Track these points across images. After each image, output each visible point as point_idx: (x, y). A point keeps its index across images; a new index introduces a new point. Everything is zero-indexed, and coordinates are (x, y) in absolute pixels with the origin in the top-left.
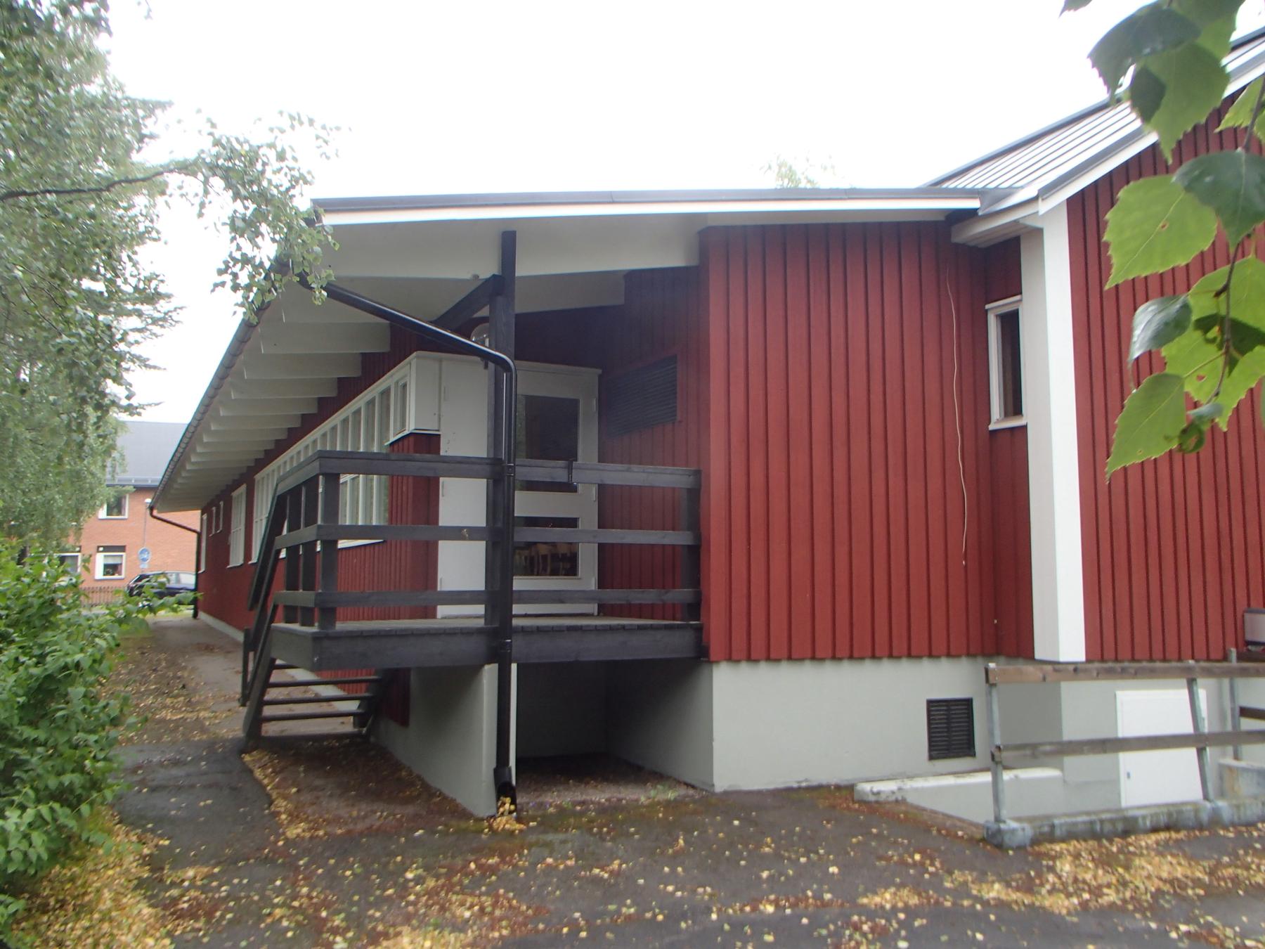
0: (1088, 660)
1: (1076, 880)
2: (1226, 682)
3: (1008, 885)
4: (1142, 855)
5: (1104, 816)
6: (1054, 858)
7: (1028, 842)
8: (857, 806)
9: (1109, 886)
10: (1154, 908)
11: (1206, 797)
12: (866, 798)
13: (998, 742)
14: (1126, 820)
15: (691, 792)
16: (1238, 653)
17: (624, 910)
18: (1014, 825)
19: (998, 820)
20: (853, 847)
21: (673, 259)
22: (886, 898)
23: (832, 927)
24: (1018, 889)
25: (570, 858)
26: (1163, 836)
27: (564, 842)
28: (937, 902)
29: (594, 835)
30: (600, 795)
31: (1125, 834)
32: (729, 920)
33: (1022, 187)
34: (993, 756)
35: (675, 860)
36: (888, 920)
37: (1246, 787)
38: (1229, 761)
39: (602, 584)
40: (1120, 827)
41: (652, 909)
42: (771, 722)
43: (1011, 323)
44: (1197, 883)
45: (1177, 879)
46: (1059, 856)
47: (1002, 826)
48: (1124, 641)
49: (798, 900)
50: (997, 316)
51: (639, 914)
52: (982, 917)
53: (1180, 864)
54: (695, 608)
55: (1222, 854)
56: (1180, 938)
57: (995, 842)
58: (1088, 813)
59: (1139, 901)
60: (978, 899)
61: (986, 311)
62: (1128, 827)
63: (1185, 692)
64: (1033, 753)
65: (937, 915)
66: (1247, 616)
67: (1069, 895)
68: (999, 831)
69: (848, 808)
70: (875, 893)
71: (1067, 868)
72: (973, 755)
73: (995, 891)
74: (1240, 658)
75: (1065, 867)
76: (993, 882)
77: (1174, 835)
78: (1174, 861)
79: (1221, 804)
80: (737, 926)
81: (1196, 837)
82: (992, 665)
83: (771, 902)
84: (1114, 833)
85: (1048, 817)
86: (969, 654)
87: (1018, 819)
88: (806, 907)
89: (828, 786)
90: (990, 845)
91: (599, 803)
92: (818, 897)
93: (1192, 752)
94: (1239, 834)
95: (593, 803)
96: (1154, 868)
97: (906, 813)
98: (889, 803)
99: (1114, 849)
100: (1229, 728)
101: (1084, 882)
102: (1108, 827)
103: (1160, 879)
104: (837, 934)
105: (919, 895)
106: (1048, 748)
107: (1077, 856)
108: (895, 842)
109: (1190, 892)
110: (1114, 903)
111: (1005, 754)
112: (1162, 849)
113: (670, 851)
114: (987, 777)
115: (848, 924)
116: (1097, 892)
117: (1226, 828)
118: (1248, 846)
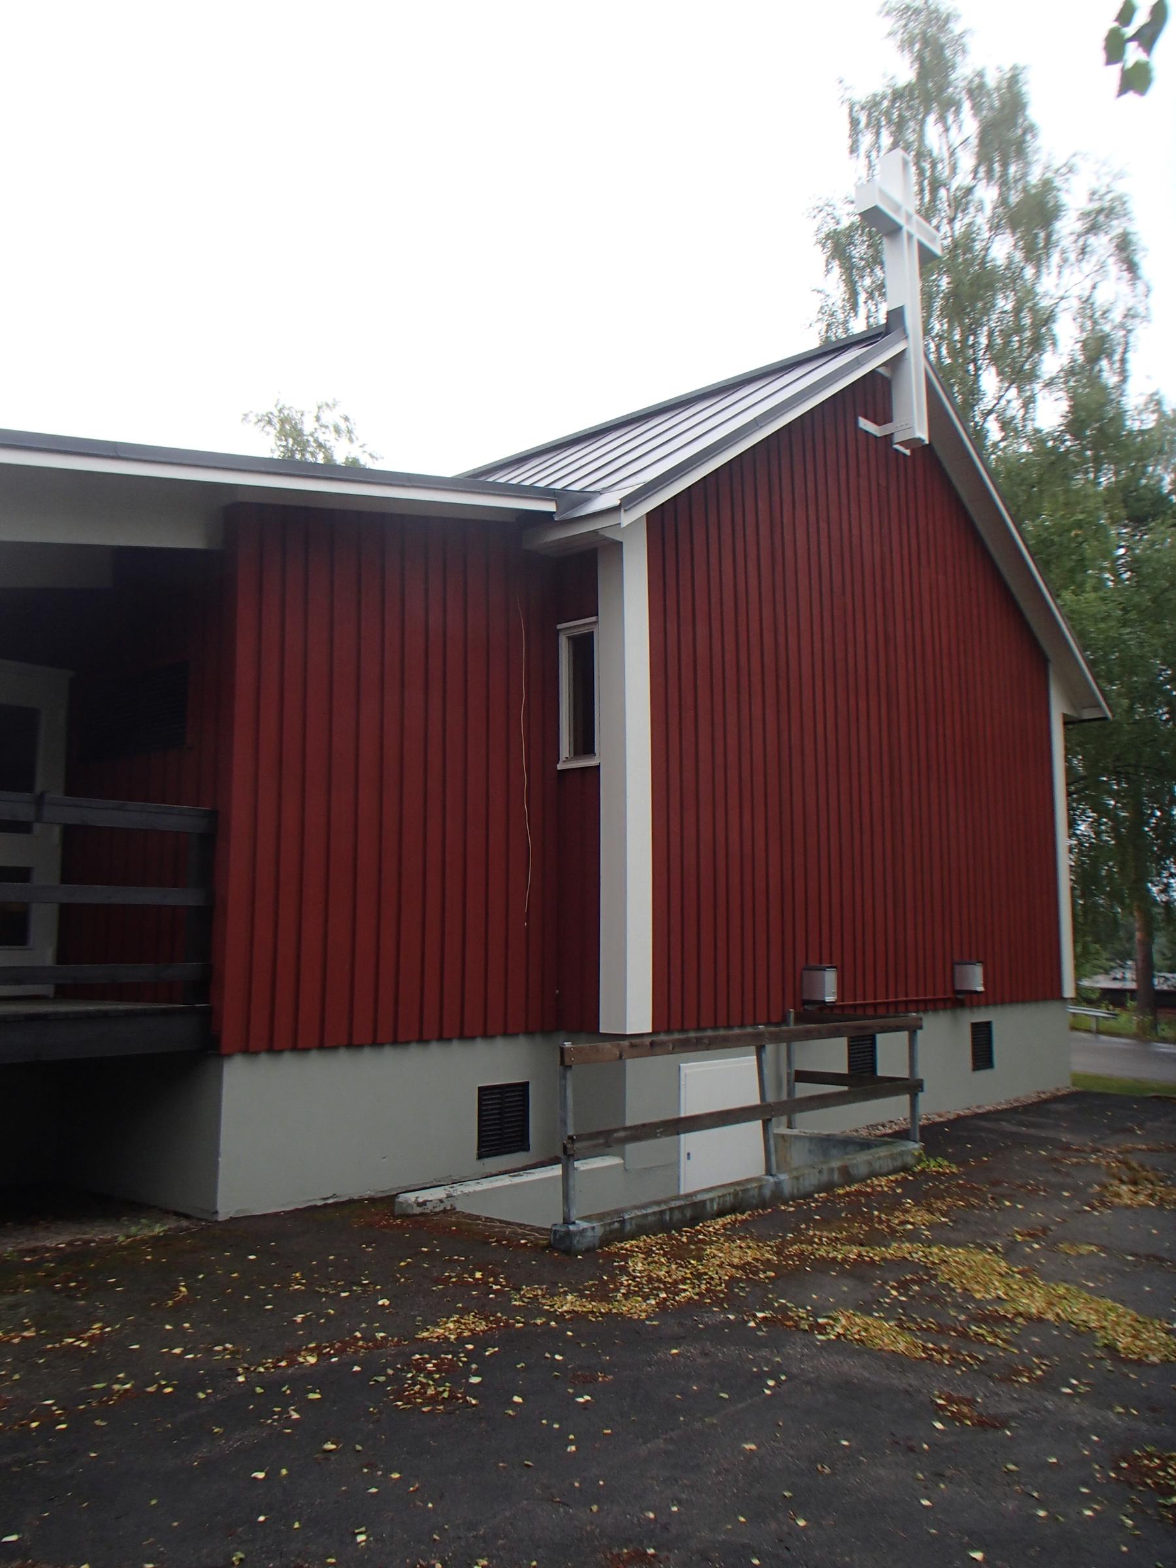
0: (655, 1031)
1: (650, 1280)
2: (783, 1046)
3: (582, 1295)
4: (711, 1243)
5: (673, 1204)
6: (625, 1258)
7: (597, 1243)
8: (398, 1221)
9: (684, 1280)
10: (730, 1300)
11: (769, 1172)
12: (410, 1211)
13: (571, 1132)
14: (694, 1205)
15: (185, 1223)
16: (796, 1014)
17: (116, 1387)
18: (584, 1225)
19: (567, 1221)
20: (402, 1270)
21: (186, 537)
22: (449, 1328)
23: (390, 1372)
24: (592, 1298)
25: (27, 1328)
26: (729, 1218)
27: (14, 1307)
28: (507, 1325)
29: (57, 1292)
30: (58, 1239)
31: (693, 1222)
32: (261, 1380)
33: (600, 493)
34: (565, 1147)
35: (179, 1312)
36: (455, 1354)
37: (798, 1156)
38: (783, 1130)
39: (62, 957)
40: (688, 1213)
41: (155, 1381)
42: (296, 1128)
43: (584, 648)
44: (768, 1264)
45: (748, 1263)
46: (629, 1254)
47: (571, 1227)
48: (692, 1013)
49: (346, 1345)
50: (569, 638)
51: (138, 1390)
52: (558, 1334)
53: (749, 1247)
54: (204, 986)
55: (786, 1231)
56: (758, 1327)
57: (562, 1247)
58: (658, 1203)
59: (715, 1292)
60: (551, 1315)
61: (558, 632)
62: (695, 1212)
63: (753, 1059)
64: (607, 1139)
65: (508, 1338)
66: (805, 973)
67: (646, 1298)
68: (569, 1234)
69: (389, 1226)
70: (437, 1325)
71: (640, 1267)
72: (527, 1149)
73: (569, 1303)
74: (799, 1019)
75: (638, 1265)
76: (565, 1293)
77: (740, 1217)
78: (743, 1245)
79: (783, 1177)
80: (272, 1385)
81: (760, 1215)
82: (567, 1044)
83: (311, 1351)
84: (682, 1222)
85: (618, 1212)
86: (529, 1032)
87: (587, 1218)
88: (356, 1352)
89: (361, 1200)
90: (558, 1253)
91: (57, 1249)
92: (368, 1337)
93: (758, 1124)
94: (798, 1206)
95: (48, 1250)
96: (727, 1256)
97: (457, 1224)
98: (436, 1214)
99: (684, 1239)
100: (784, 1097)
101: (659, 1280)
102: (677, 1215)
103: (733, 1266)
104: (397, 1379)
105: (486, 1319)
106: (622, 1134)
107: (648, 1253)
108: (451, 1261)
109: (762, 1276)
110: (691, 1298)
111: (577, 1145)
112: (731, 1233)
113: (170, 1303)
114: (557, 1171)
115: (409, 1365)
116: (673, 1288)
117: (786, 1203)
118: (808, 1220)
